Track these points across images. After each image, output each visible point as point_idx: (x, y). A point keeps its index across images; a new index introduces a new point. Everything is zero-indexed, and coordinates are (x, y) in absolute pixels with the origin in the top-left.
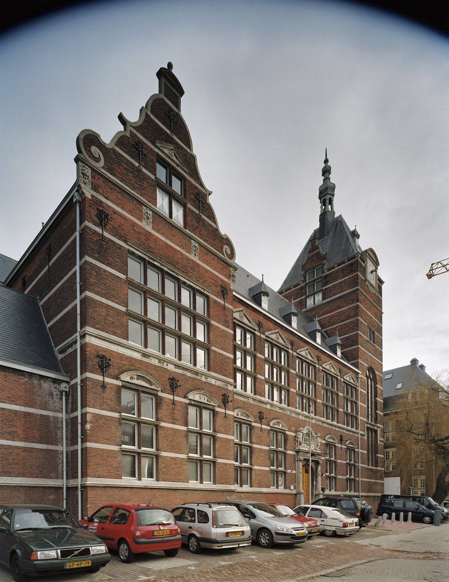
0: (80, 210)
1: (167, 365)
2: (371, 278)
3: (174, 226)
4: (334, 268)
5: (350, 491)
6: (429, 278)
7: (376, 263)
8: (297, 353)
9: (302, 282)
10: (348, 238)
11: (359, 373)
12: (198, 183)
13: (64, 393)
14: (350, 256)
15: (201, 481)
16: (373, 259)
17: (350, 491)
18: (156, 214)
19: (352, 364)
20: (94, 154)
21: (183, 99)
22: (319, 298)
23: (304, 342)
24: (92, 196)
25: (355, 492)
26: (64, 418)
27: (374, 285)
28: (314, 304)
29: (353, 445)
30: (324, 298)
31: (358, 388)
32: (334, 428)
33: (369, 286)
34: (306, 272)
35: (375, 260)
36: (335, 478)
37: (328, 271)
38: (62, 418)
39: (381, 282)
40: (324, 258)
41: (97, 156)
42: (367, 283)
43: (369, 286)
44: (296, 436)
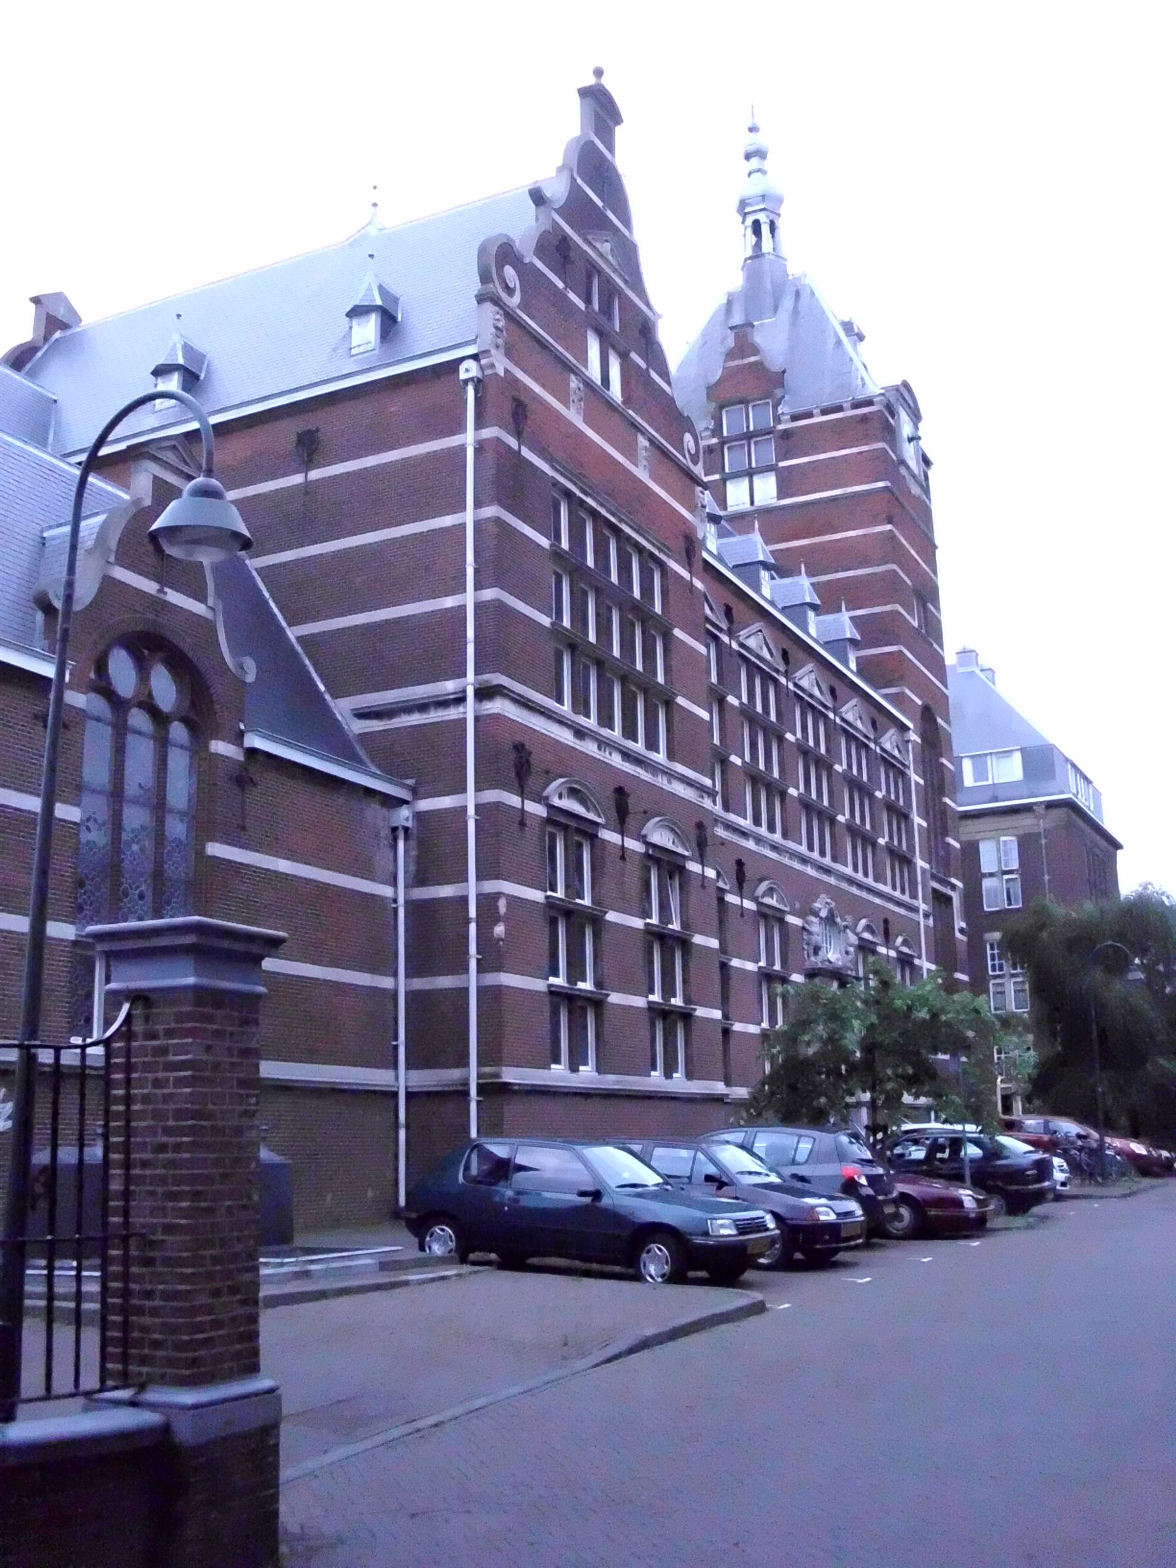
0: (478, 401)
1: (610, 754)
2: (909, 453)
3: (610, 405)
4: (809, 415)
5: (668, 1074)
6: (780, 200)
7: (916, 416)
8: (796, 685)
9: (708, 433)
10: (839, 342)
11: (908, 729)
12: (641, 298)
13: (401, 835)
14: (860, 397)
15: (570, 1063)
16: (909, 405)
17: (668, 1074)
18: (588, 384)
19: (885, 697)
20: (508, 281)
21: (619, 130)
22: (766, 490)
23: (805, 650)
24: (506, 371)
25: (689, 1075)
26: (401, 900)
27: (916, 472)
28: (752, 503)
29: (872, 932)
30: (782, 493)
31: (907, 771)
32: (786, 860)
33: (908, 477)
34: (721, 407)
35: (912, 405)
36: (598, 1003)
37: (794, 418)
38: (395, 901)
39: (927, 462)
40: (779, 379)
41: (511, 285)
42: (903, 471)
43: (908, 477)
44: (803, 928)
